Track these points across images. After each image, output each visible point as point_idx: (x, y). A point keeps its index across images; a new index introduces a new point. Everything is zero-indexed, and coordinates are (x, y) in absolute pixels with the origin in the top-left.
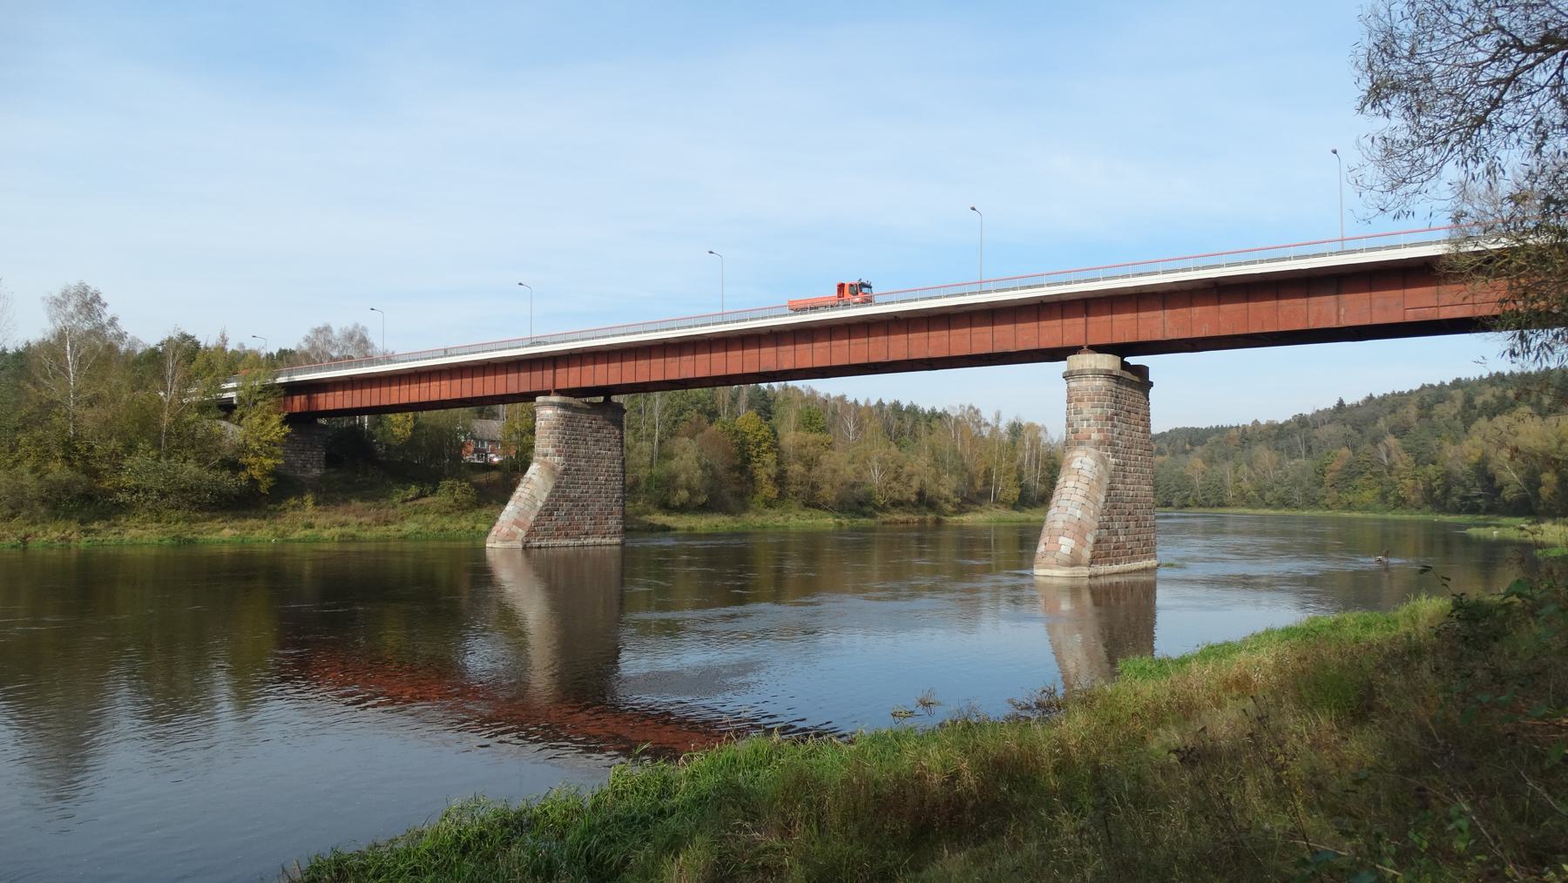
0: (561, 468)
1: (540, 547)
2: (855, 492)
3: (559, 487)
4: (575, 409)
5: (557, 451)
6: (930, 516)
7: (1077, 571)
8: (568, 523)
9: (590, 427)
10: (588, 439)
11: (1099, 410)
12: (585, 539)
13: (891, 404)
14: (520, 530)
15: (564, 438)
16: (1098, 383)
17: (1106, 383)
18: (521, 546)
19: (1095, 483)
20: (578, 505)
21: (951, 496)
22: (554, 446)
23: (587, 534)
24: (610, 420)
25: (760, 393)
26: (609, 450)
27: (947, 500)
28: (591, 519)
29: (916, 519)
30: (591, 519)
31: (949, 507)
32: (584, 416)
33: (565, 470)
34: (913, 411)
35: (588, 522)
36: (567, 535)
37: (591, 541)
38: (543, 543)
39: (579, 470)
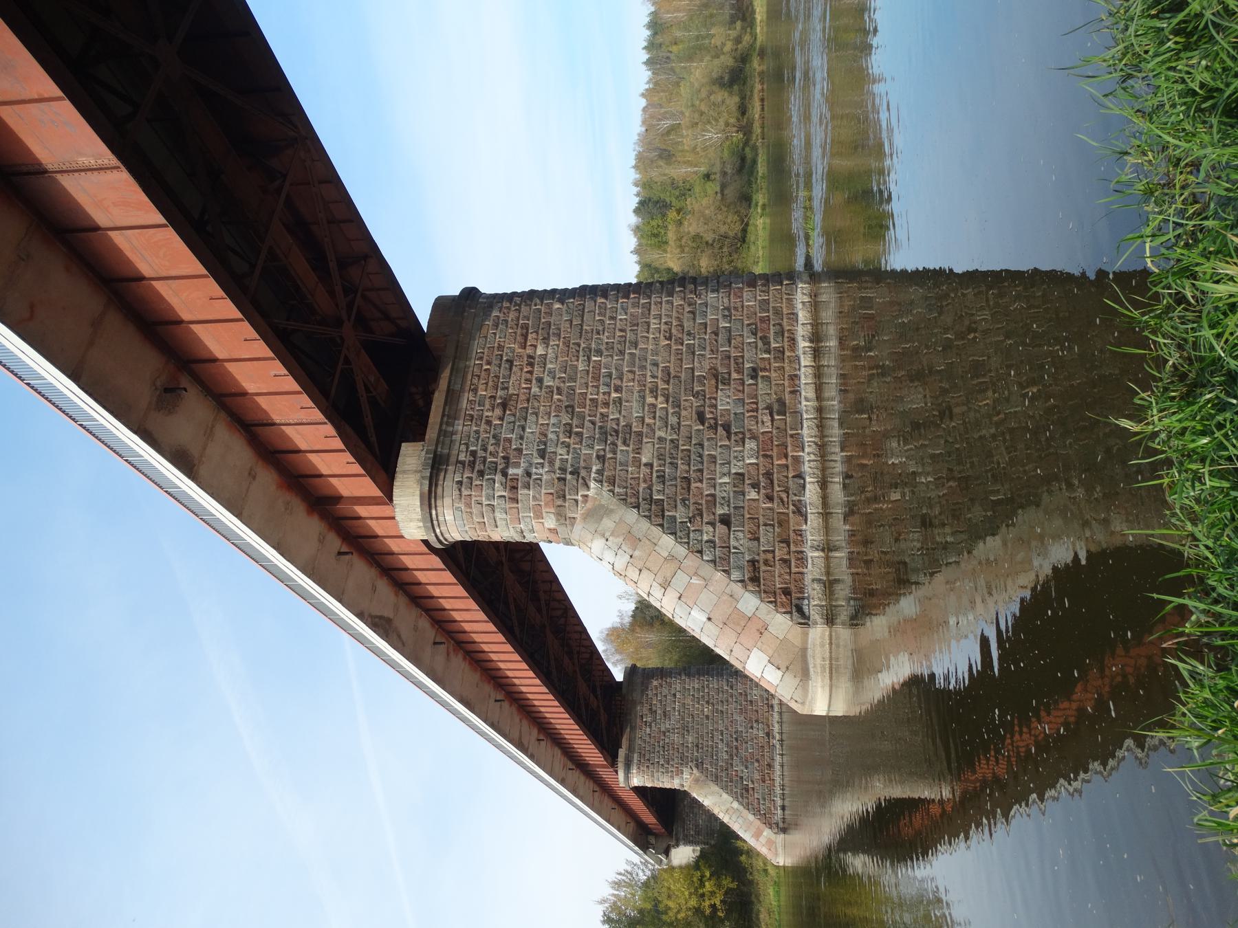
0: (695, 771)
1: (783, 808)
2: (730, 171)
3: (717, 777)
4: (631, 749)
5: (677, 775)
6: (756, 64)
7: (819, 661)
8: (756, 764)
9: (650, 726)
10: (663, 729)
11: (498, 515)
12: (774, 738)
13: (648, 53)
14: (765, 834)
15: (662, 765)
16: (449, 518)
17: (447, 501)
18: (782, 836)
19: (637, 553)
20: (737, 748)
21: (733, 34)
22: (672, 777)
23: (768, 734)
24: (643, 692)
25: (642, 208)
26: (675, 695)
27: (738, 40)
28: (752, 728)
29: (758, 87)
30: (752, 728)
31: (747, 38)
32: (639, 734)
33: (697, 767)
34: (651, 46)
35: (755, 731)
36: (770, 766)
37: (776, 728)
38: (779, 802)
39: (697, 746)
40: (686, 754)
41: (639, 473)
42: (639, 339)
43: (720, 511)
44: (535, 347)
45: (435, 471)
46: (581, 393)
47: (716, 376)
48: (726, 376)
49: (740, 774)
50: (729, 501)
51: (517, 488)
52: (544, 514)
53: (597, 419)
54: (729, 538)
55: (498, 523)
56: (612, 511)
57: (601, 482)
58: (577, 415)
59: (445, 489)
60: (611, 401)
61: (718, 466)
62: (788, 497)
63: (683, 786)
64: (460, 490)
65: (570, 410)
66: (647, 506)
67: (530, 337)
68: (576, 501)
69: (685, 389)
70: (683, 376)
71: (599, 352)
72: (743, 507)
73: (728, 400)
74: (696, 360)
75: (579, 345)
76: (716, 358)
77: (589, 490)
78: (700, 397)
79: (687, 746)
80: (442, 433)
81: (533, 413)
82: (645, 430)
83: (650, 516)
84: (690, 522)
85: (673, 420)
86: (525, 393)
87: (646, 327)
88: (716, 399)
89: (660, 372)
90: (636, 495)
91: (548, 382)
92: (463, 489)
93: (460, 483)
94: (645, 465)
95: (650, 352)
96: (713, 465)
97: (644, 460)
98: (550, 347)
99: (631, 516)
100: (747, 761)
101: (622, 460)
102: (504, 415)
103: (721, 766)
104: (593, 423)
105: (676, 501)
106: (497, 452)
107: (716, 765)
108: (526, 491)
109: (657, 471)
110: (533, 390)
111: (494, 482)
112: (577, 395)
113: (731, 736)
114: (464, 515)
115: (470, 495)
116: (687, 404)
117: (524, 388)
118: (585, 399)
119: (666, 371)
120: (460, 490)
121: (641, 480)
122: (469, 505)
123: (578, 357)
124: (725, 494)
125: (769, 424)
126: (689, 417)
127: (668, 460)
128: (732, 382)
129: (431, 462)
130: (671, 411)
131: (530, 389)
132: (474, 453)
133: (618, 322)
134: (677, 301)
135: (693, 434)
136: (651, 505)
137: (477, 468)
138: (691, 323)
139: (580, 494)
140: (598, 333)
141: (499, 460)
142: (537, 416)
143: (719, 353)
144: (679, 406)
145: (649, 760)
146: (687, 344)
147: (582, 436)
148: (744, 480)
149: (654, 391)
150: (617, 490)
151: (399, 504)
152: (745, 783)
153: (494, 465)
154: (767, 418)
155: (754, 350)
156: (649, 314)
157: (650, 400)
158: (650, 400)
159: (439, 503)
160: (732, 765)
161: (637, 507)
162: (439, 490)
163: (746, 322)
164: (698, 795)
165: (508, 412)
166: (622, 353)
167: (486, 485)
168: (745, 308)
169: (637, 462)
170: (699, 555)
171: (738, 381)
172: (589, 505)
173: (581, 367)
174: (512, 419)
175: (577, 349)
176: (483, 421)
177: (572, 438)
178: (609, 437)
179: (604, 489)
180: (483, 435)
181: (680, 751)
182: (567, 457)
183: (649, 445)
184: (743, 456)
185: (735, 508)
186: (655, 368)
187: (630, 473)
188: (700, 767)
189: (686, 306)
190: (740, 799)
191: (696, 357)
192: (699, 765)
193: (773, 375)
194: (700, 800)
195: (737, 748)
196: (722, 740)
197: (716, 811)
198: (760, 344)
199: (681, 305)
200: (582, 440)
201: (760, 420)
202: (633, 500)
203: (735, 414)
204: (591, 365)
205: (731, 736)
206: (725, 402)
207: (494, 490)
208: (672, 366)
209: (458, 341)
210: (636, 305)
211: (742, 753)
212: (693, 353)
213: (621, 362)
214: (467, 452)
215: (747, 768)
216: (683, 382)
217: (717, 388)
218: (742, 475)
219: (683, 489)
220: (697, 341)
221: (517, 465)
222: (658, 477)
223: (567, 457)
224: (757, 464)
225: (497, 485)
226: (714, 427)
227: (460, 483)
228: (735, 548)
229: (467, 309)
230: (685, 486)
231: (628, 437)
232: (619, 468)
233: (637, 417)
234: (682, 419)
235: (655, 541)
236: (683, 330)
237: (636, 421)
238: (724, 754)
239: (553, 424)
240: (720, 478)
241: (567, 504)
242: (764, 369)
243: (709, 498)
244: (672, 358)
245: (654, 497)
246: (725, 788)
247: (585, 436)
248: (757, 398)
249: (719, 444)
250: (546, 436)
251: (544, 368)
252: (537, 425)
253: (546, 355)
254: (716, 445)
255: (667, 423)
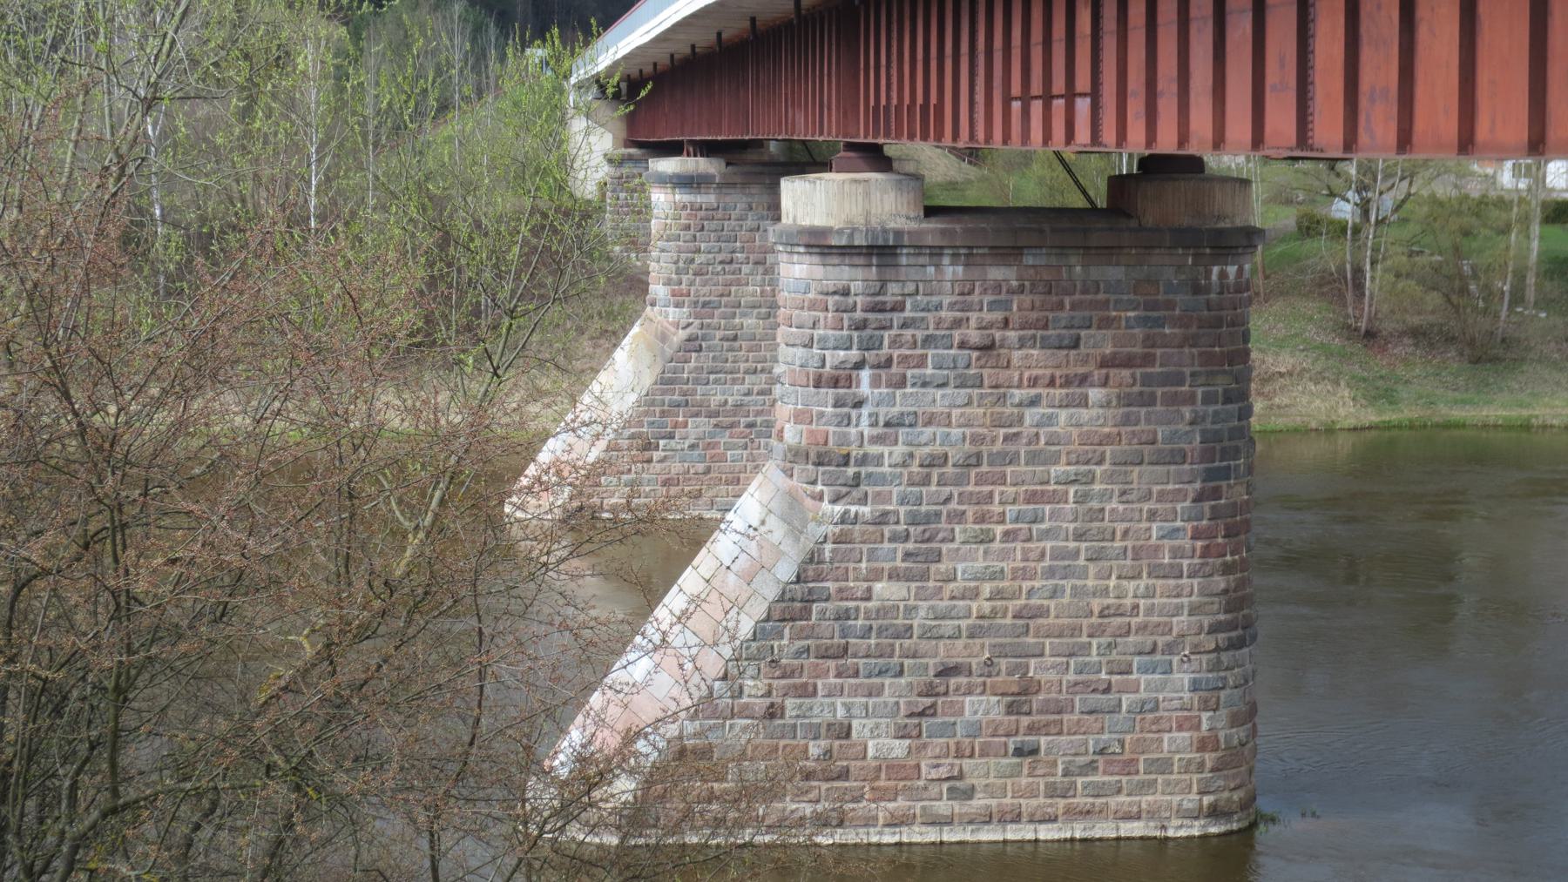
0: (683, 334)
3: (671, 382)
17: (819, 271)
20: (732, 426)
22: (668, 283)
40: (717, 312)
41: (856, 579)
42: (1106, 564)
43: (790, 703)
44: (1105, 384)
45: (864, 251)
46: (1005, 475)
47: (1024, 692)
48: (1025, 708)
49: (679, 432)
50: (805, 717)
51: (835, 387)
52: (800, 427)
53: (953, 505)
54: (747, 717)
55: (790, 349)
56: (797, 540)
57: (843, 521)
58: (962, 474)
59: (837, 268)
60: (989, 526)
61: (864, 700)
62: (810, 801)
63: (653, 304)
64: (835, 293)
65: (973, 461)
66: (799, 596)
67: (1126, 373)
68: (814, 483)
69: (1001, 645)
70: (1030, 640)
71: (1082, 499)
72: (795, 737)
73: (980, 712)
74: (1059, 660)
75: (1100, 463)
76: (1060, 691)
77: (830, 502)
78: (987, 669)
79: (734, 316)
80: (938, 251)
81: (970, 397)
82: (931, 584)
83: (783, 601)
84: (773, 661)
85: (948, 626)
86: (1011, 378)
87: (1130, 575)
88: (983, 693)
89: (1039, 602)
90: (819, 578)
91: (1031, 415)
92: (837, 297)
93: (846, 292)
94: (869, 590)
95: (1079, 583)
96: (866, 693)
97: (878, 587)
98: (1101, 411)
99: (786, 571)
100: (709, 446)
101: (880, 553)
102: (970, 348)
103: (694, 393)
104: (948, 500)
105: (807, 638)
106: (900, 347)
107: (697, 381)
108: (831, 401)
109: (857, 609)
110: (1016, 391)
111: (847, 349)
112: (1003, 469)
113: (758, 413)
114: (800, 296)
115: (827, 310)
116: (976, 649)
117: (1021, 375)
118: (993, 484)
119: (1042, 612)
120: (835, 293)
121: (843, 584)
122: (813, 306)
123: (1077, 463)
124: (816, 711)
125: (934, 774)
126: (954, 652)
127: (875, 624)
128: (1013, 718)
129: (880, 242)
130: (964, 623)
131: (1019, 386)
132: (898, 307)
133: (1144, 525)
134: (1181, 622)
135: (922, 660)
136: (801, 601)
137: (871, 316)
138: (1132, 650)
139: (824, 488)
140: (1123, 493)
141: (885, 350)
142: (967, 405)
143: (1070, 697)
144: (971, 636)
145: (702, 229)
146: (1090, 643)
147: (924, 485)
148: (838, 738)
149: (997, 595)
150: (828, 547)
151: (815, 189)
152: (662, 442)
153: (877, 344)
154: (943, 772)
155: (1073, 751)
156: (1157, 577)
157: (987, 588)
158: (987, 588)
159: (816, 259)
160: (697, 415)
161: (798, 580)
162: (836, 260)
163: (1128, 737)
164: (634, 337)
165: (975, 354)
166: (1079, 536)
167: (842, 337)
168: (1156, 736)
169: (876, 575)
170: (721, 674)
171: (1014, 727)
172: (809, 502)
173: (1056, 470)
174: (961, 363)
175: (1093, 461)
176: (959, 314)
177: (920, 469)
178: (921, 528)
179: (831, 527)
180: (931, 317)
181: (724, 299)
182: (886, 464)
183: (904, 593)
184: (879, 736)
185: (795, 726)
186: (1047, 594)
187: (857, 565)
188: (691, 345)
189: (1168, 638)
190: (627, 433)
191: (1065, 659)
192: (693, 344)
193: (1024, 781)
194: (626, 341)
195: (732, 426)
196: (749, 393)
197: (603, 377)
198: (1082, 760)
199: (1171, 629)
200: (918, 485)
201: (943, 761)
202: (811, 573)
203: (954, 724)
204: (1060, 487)
205: (758, 413)
206: (980, 708)
207: (835, 349)
208: (1051, 620)
209: (1121, 247)
210: (1177, 553)
211: (725, 438)
212: (1071, 655)
213: (1063, 535)
214: (903, 295)
215: (693, 447)
216: (1016, 640)
217: (1003, 694)
218: (848, 735)
219: (826, 650)
220: (1096, 659)
221: (875, 382)
222: (847, 610)
223: (886, 464)
224: (865, 757)
225: (842, 353)
226: (930, 691)
227: (846, 292)
228: (731, 726)
229: (1191, 251)
230: (831, 652)
231: (919, 559)
232: (865, 547)
233: (955, 570)
234: (948, 642)
235: (747, 608)
236: (1120, 636)
237: (947, 570)
238: (719, 398)
239: (949, 434)
240: (844, 704)
241: (810, 467)
242: (1033, 768)
243: (811, 689)
244: (1066, 621)
245: (815, 605)
246: (648, 402)
247: (924, 489)
248: (981, 756)
249: (902, 701)
250: (928, 423)
251: (1060, 406)
252: (950, 406)
253: (1086, 406)
254: (900, 696)
255: (943, 618)
